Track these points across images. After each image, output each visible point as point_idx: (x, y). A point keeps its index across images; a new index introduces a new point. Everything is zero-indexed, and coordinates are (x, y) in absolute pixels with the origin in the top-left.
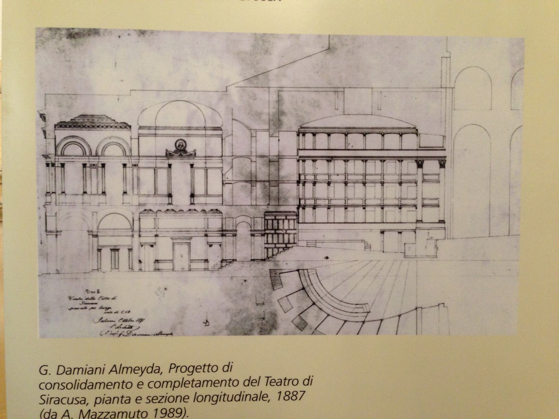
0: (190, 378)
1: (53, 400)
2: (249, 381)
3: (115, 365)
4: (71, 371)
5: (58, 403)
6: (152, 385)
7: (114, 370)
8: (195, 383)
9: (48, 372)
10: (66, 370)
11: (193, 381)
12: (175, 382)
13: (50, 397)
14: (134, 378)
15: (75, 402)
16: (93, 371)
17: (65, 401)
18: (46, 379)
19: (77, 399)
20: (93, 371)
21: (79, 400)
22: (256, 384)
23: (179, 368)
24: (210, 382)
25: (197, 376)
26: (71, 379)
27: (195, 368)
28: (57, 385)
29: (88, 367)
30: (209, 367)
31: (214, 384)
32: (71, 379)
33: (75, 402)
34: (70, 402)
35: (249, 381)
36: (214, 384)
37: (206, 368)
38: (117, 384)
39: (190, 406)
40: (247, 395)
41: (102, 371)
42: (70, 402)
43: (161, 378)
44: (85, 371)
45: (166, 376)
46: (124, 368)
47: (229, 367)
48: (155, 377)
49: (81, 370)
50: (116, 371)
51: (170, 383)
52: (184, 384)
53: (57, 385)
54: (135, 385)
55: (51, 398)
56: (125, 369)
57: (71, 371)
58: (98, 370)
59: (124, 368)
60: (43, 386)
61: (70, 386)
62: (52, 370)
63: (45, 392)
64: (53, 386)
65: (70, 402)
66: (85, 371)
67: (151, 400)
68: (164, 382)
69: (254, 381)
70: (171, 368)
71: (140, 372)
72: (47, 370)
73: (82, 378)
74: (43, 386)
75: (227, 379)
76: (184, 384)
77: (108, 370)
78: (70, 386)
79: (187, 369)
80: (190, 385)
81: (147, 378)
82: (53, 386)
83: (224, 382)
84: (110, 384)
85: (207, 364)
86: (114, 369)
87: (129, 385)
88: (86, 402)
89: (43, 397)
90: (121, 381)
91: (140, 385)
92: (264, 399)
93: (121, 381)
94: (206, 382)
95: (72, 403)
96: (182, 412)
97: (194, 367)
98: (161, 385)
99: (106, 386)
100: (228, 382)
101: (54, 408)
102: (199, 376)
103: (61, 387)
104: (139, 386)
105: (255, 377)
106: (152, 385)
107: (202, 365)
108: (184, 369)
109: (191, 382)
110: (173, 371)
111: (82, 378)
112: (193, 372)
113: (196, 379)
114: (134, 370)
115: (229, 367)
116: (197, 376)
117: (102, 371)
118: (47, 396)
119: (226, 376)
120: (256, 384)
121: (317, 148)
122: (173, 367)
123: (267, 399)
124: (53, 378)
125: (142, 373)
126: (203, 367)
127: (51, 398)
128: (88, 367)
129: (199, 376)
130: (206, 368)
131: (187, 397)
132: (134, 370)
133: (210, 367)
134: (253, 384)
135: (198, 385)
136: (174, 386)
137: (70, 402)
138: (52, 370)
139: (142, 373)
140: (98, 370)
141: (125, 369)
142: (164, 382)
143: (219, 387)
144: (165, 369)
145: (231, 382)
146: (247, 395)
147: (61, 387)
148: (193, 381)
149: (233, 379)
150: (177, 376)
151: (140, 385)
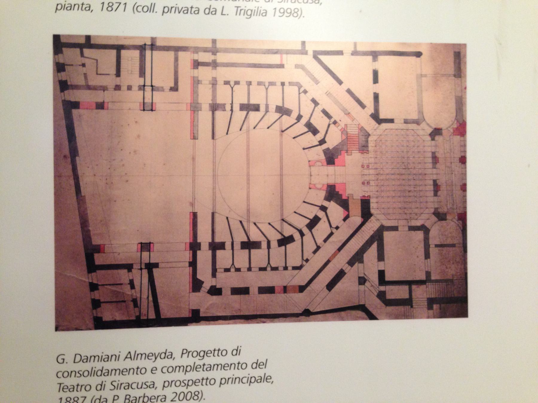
0: (201, 363)
1: (123, 386)
2: (257, 364)
3: (130, 352)
4: (87, 359)
5: (128, 388)
6: (165, 370)
7: (129, 356)
8: (205, 367)
9: (65, 362)
10: (83, 358)
11: (204, 365)
12: (187, 366)
13: (120, 383)
14: (148, 364)
15: (144, 386)
16: (109, 358)
17: (134, 386)
18: (63, 367)
19: (147, 384)
20: (109, 358)
21: (148, 384)
22: (264, 367)
23: (191, 353)
24: (220, 366)
25: (208, 361)
26: (87, 366)
27: (206, 353)
28: (73, 374)
29: (104, 355)
30: (218, 352)
31: (223, 367)
32: (87, 366)
33: (144, 386)
34: (139, 386)
35: (257, 364)
36: (223, 367)
37: (216, 352)
38: (132, 371)
39: (206, 389)
40: (236, 378)
41: (117, 358)
42: (139, 387)
43: (174, 363)
44: (101, 359)
45: (179, 361)
46: (138, 355)
47: (237, 351)
48: (168, 362)
49: (97, 358)
50: (131, 358)
51: (182, 368)
52: (195, 368)
53: (73, 374)
54: (149, 370)
55: (121, 384)
56: (140, 356)
57: (87, 359)
58: (114, 357)
59: (138, 355)
60: (60, 375)
61: (86, 374)
62: (69, 358)
63: (62, 380)
64: (70, 374)
65: (139, 387)
66: (101, 359)
67: (167, 384)
68: (176, 367)
69: (262, 364)
70: (183, 354)
71: (153, 358)
72: (64, 359)
73: (98, 365)
74: (60, 375)
75: (236, 363)
76: (195, 368)
77: (122, 357)
78: (86, 374)
79: (198, 354)
80: (201, 369)
81: (160, 363)
82: (70, 374)
83: (132, 371)
84: (227, 365)
85: (217, 349)
86: (129, 356)
87: (143, 371)
88: (155, 387)
89: (114, 383)
90: (135, 368)
91: (153, 370)
92: (268, 380)
93: (135, 368)
94: (216, 366)
95: (141, 388)
96: (197, 395)
97: (204, 352)
98: (174, 369)
99: (122, 372)
100: (136, 370)
101: (73, 395)
102: (209, 360)
103: (78, 375)
104: (153, 372)
105: (262, 360)
106: (165, 370)
107: (212, 349)
108: (195, 354)
109: (202, 367)
110: (185, 356)
111: (98, 365)
112: (204, 356)
113: (206, 364)
114: (147, 356)
115: (237, 351)
116: (208, 361)
117: (117, 358)
118: (118, 382)
119: (235, 360)
120: (264, 367)
121: (154, 92)
122: (185, 352)
123: (271, 381)
124: (70, 366)
125: (156, 358)
126: (213, 352)
127: (121, 384)
128: (104, 355)
129: (209, 360)
130: (216, 352)
131: (269, 378)
132: (147, 356)
133: (220, 352)
134: (261, 367)
135: (208, 369)
136: (186, 371)
137: (139, 386)
138: (69, 358)
139: (156, 358)
140: (114, 357)
141: (140, 356)
142: (176, 367)
143: (127, 376)
144: (177, 354)
145: (239, 365)
146: (236, 378)
147: (78, 375)
148: (204, 365)
149: (140, 367)
150: (188, 361)
151: (153, 370)
